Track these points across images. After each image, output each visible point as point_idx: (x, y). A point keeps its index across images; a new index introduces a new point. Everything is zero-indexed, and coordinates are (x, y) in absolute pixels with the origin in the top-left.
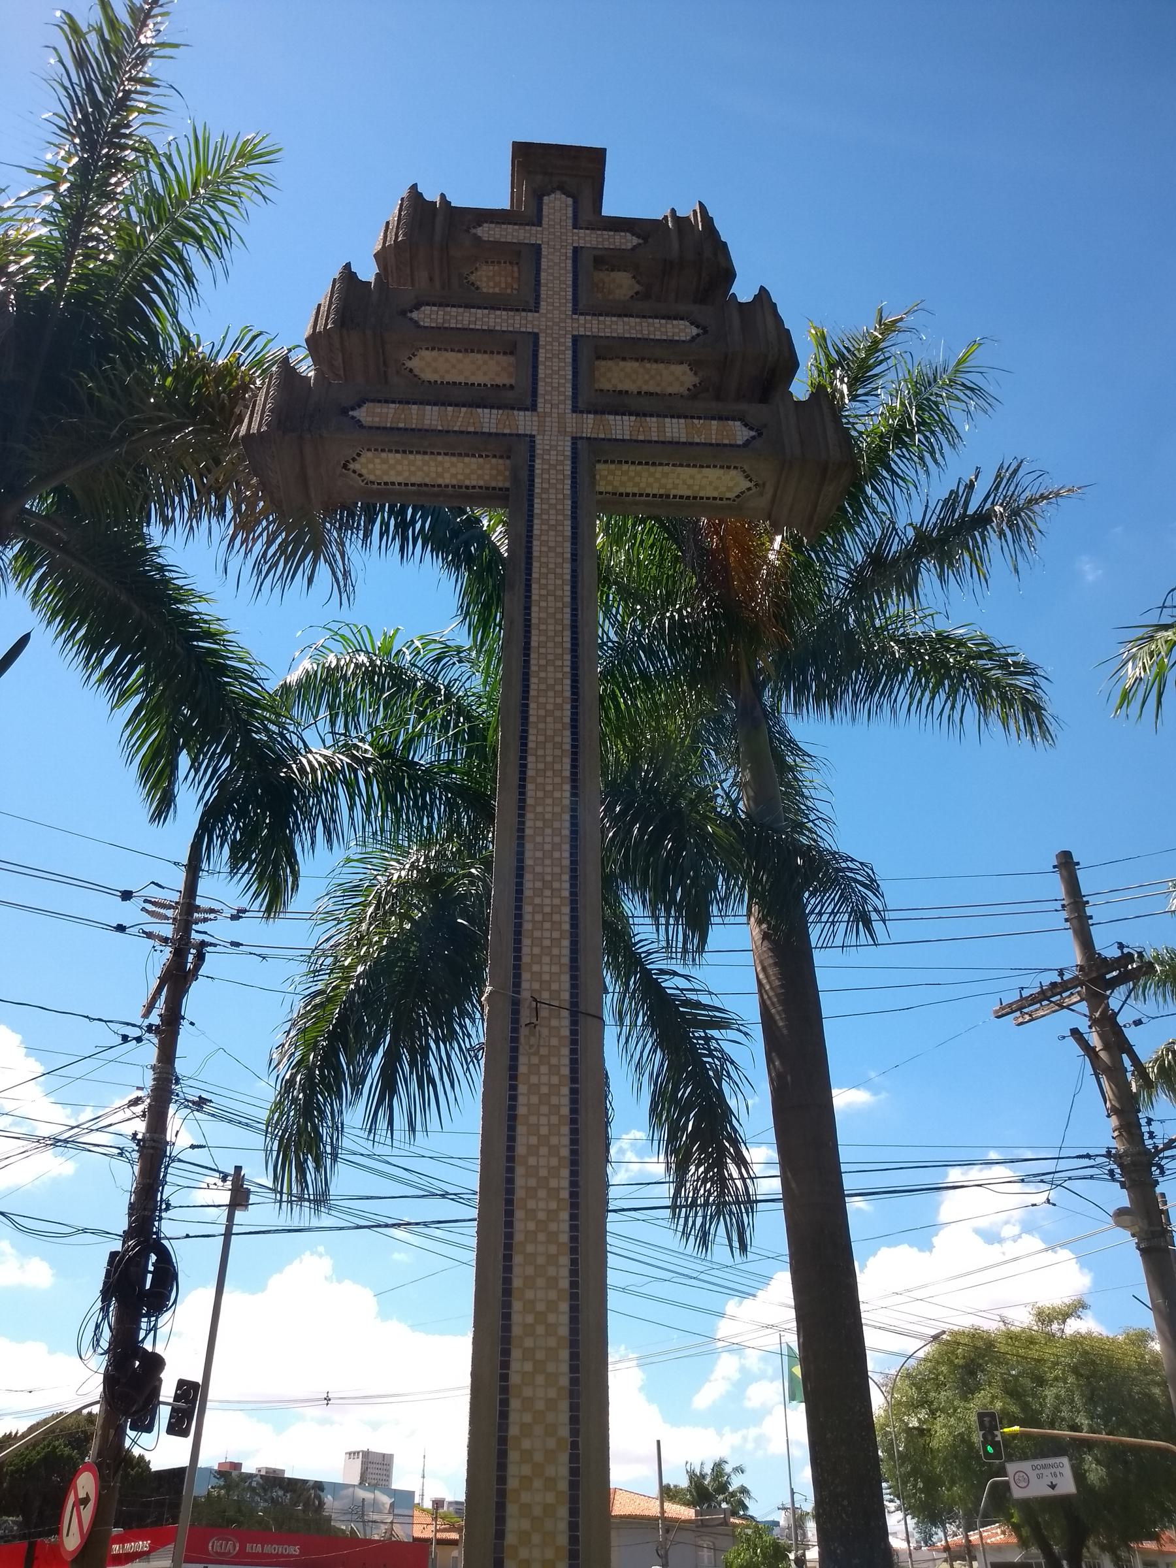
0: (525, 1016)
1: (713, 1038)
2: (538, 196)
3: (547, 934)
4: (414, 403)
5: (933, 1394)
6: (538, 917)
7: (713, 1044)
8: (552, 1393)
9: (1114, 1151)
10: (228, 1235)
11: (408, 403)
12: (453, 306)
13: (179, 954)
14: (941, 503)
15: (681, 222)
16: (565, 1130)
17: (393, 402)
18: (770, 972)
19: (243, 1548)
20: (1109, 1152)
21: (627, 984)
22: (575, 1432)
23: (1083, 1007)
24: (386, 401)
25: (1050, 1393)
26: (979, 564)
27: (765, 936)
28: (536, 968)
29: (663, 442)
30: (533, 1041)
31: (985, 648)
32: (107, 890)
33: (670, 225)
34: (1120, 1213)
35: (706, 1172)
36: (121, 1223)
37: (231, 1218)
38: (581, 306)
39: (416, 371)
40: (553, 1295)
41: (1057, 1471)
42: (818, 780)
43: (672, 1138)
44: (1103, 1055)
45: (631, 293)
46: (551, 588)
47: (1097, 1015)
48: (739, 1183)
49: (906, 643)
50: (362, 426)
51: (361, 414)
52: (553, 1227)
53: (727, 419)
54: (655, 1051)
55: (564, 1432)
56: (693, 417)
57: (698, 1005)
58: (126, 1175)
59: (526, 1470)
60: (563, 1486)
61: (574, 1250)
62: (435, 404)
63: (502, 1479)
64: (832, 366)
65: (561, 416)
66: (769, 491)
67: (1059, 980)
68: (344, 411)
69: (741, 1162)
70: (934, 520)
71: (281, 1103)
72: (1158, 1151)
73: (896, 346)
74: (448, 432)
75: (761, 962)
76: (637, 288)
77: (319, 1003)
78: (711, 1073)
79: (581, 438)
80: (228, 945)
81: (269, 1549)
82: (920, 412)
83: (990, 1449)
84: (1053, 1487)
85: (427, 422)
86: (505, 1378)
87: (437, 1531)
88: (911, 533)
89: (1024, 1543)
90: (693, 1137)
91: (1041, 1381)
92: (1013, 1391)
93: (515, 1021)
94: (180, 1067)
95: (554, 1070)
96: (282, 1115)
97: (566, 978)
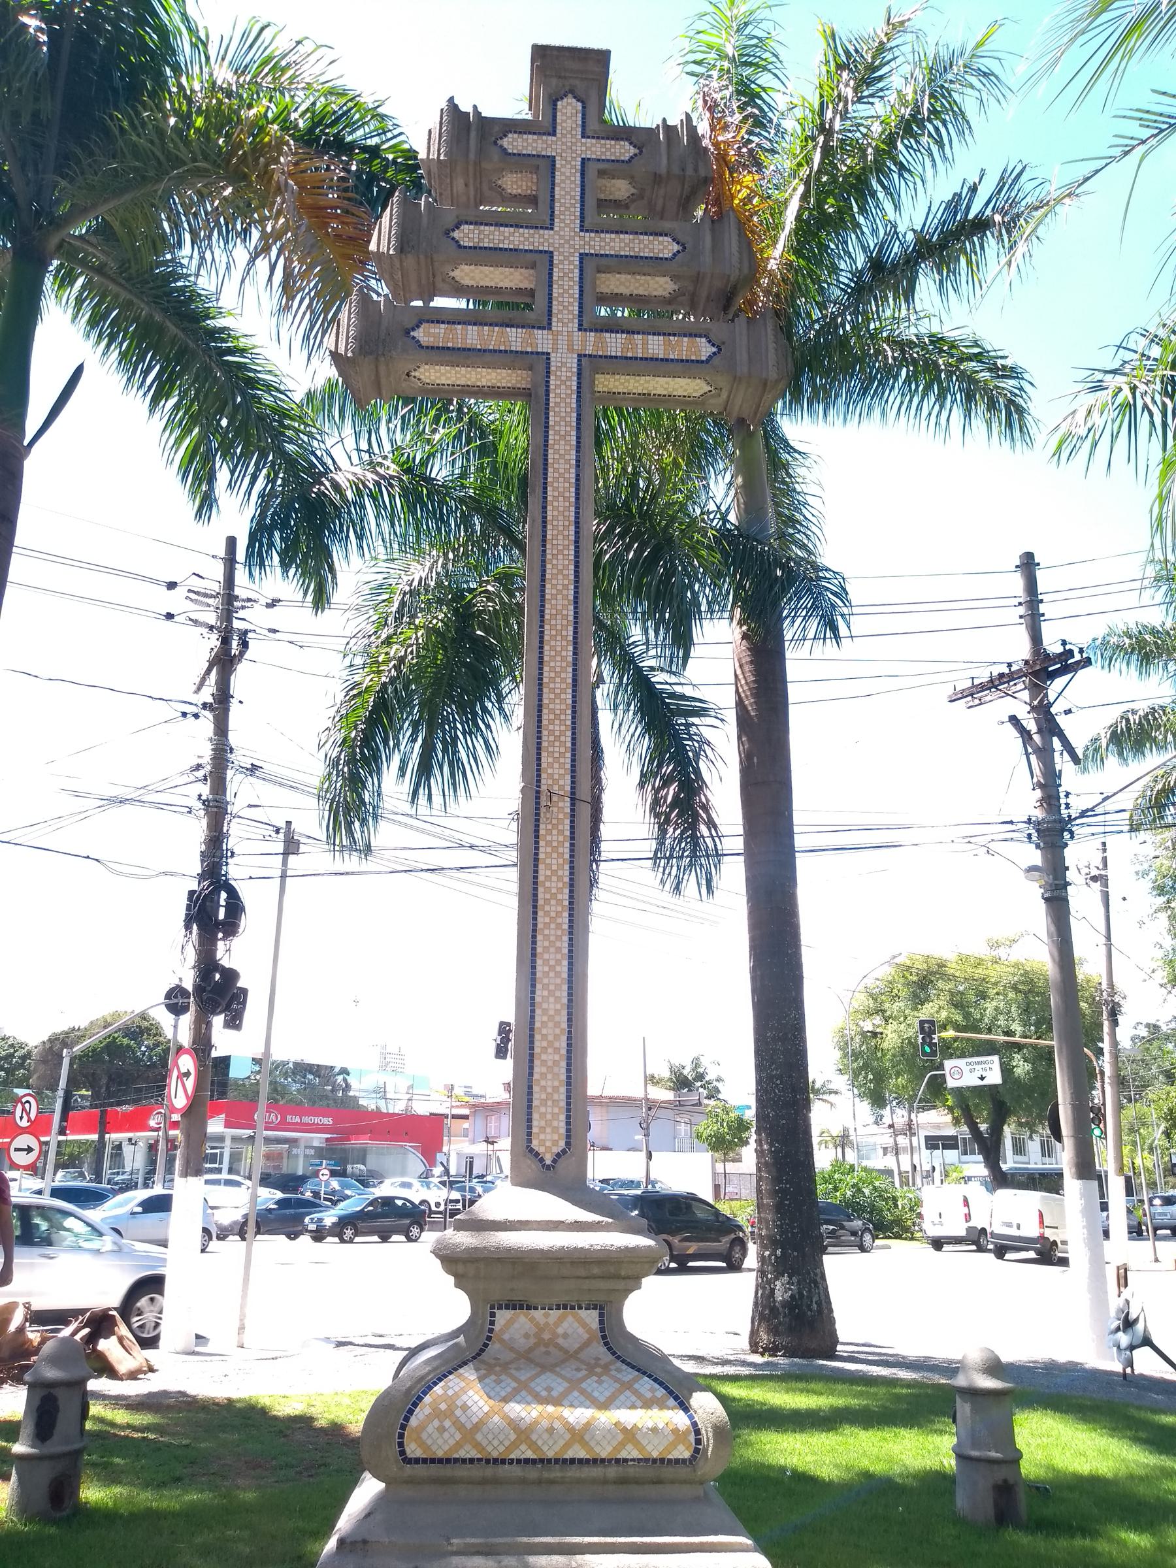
0: (544, 801)
1: (693, 724)
2: (553, 102)
3: (557, 749)
4: (459, 323)
5: (887, 1005)
6: (552, 738)
7: (693, 730)
8: (558, 1007)
9: (1034, 819)
10: (284, 876)
11: (454, 323)
12: (486, 224)
13: (225, 641)
14: (944, 205)
15: (669, 130)
16: (567, 867)
17: (443, 322)
18: (747, 668)
19: (283, 1118)
20: (1029, 819)
21: (621, 679)
22: (570, 1026)
23: (1025, 695)
24: (438, 322)
25: (990, 1006)
26: (975, 268)
27: (745, 636)
28: (550, 771)
29: (646, 359)
30: (548, 815)
31: (976, 350)
32: (155, 582)
33: (661, 136)
34: (1032, 869)
35: (682, 833)
36: (197, 868)
37: (285, 863)
38: (586, 224)
39: (457, 279)
40: (559, 956)
41: (987, 1066)
42: (809, 477)
43: (656, 802)
44: (1036, 738)
45: (628, 194)
46: (561, 490)
47: (1036, 703)
48: (709, 841)
49: (902, 345)
50: (421, 347)
51: (419, 334)
52: (559, 920)
53: (696, 336)
54: (644, 736)
55: (565, 1025)
56: (670, 334)
57: (683, 697)
58: (197, 829)
59: (544, 1044)
60: (564, 1052)
61: (571, 933)
62: (475, 324)
63: (532, 1048)
64: (840, 67)
65: (570, 334)
66: (724, 395)
67: (1006, 671)
68: (407, 332)
69: (711, 824)
70: (936, 221)
71: (330, 774)
72: (1071, 819)
73: (904, 46)
74: (485, 351)
75: (739, 660)
76: (633, 191)
77: (355, 692)
78: (690, 754)
79: (585, 355)
80: (266, 633)
81: (305, 1120)
82: (932, 101)
83: (927, 1049)
84: (982, 1078)
85: (469, 341)
86: (533, 998)
87: (452, 1107)
88: (910, 236)
89: (956, 1122)
90: (672, 806)
91: (983, 996)
92: (958, 1003)
93: (538, 803)
94: (233, 738)
95: (561, 832)
96: (330, 785)
97: (568, 777)
